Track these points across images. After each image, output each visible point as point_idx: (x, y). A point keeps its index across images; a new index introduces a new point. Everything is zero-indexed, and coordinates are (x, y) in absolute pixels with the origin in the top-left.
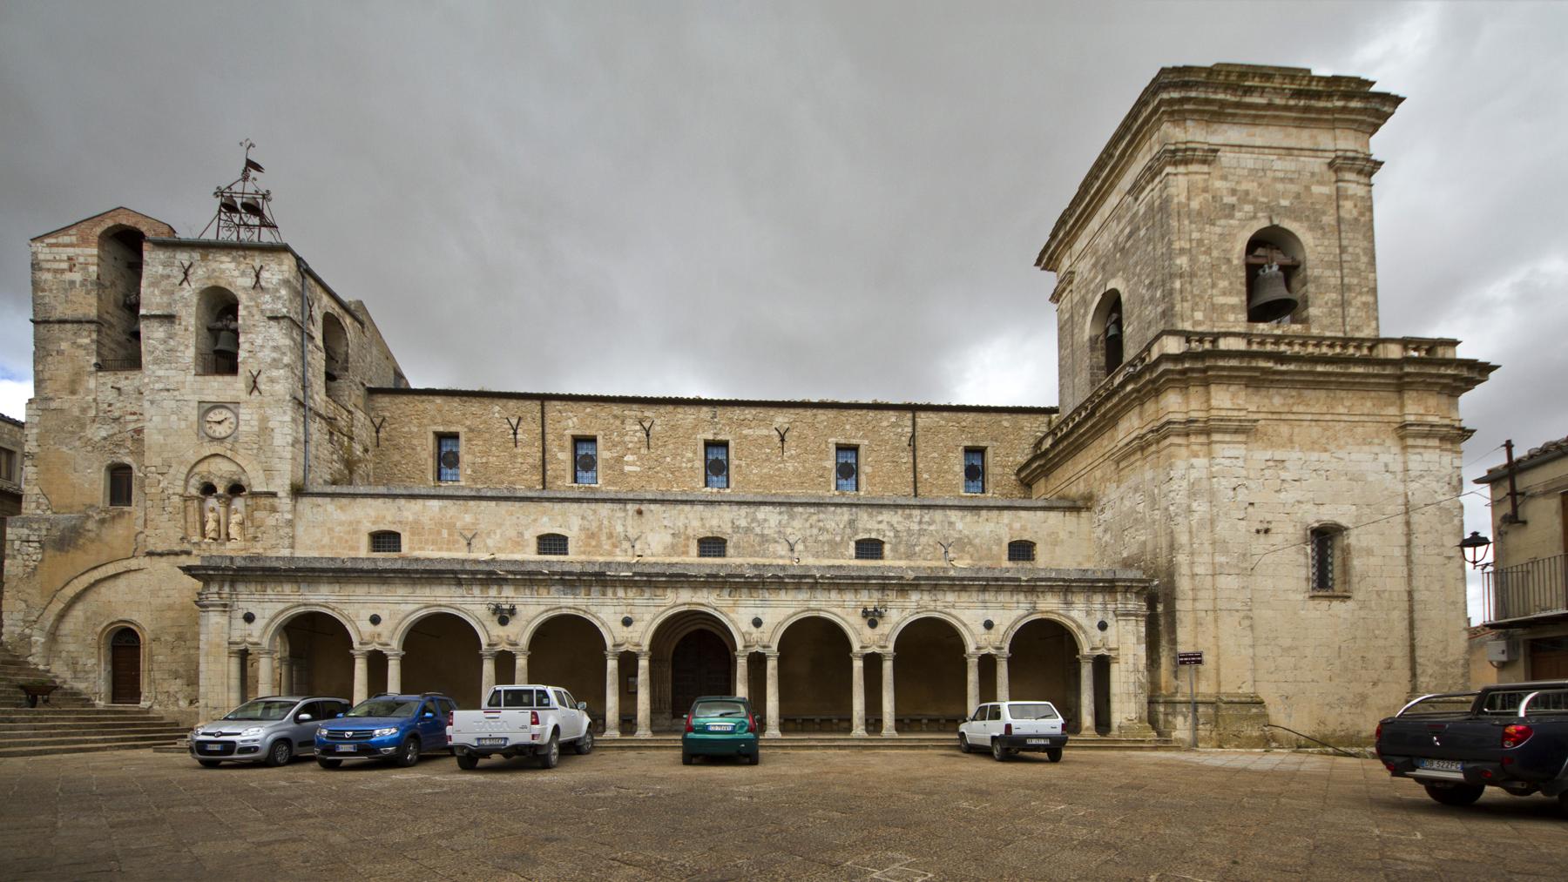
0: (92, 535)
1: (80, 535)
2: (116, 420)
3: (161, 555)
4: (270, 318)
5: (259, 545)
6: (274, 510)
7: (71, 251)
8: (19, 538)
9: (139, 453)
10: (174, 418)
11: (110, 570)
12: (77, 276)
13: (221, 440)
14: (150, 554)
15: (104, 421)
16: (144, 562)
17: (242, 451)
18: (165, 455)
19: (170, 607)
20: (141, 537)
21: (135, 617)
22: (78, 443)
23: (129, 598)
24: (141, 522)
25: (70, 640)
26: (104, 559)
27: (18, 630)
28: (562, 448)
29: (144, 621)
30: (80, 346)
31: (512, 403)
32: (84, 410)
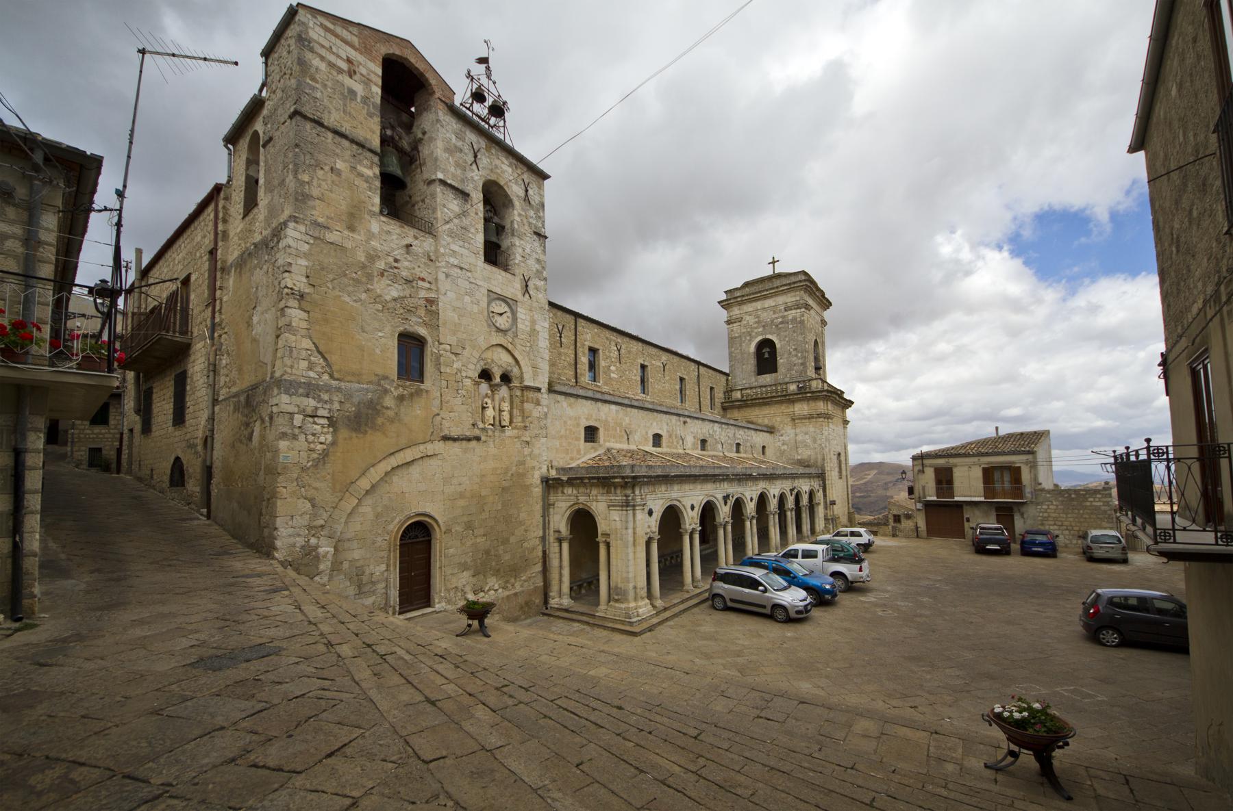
0: (390, 413)
1: (378, 412)
2: (408, 281)
3: (455, 440)
4: (535, 233)
5: (527, 433)
6: (538, 403)
7: (353, 54)
8: (302, 411)
9: (435, 327)
10: (467, 299)
11: (408, 455)
12: (359, 89)
13: (504, 332)
14: (446, 438)
15: (395, 279)
16: (439, 446)
17: (519, 347)
19: (462, 495)
20: (438, 418)
21: (429, 509)
22: (364, 296)
24: (437, 402)
25: (355, 544)
26: (403, 441)
27: (300, 541)
29: (435, 509)
30: (360, 175)
31: (559, 313)
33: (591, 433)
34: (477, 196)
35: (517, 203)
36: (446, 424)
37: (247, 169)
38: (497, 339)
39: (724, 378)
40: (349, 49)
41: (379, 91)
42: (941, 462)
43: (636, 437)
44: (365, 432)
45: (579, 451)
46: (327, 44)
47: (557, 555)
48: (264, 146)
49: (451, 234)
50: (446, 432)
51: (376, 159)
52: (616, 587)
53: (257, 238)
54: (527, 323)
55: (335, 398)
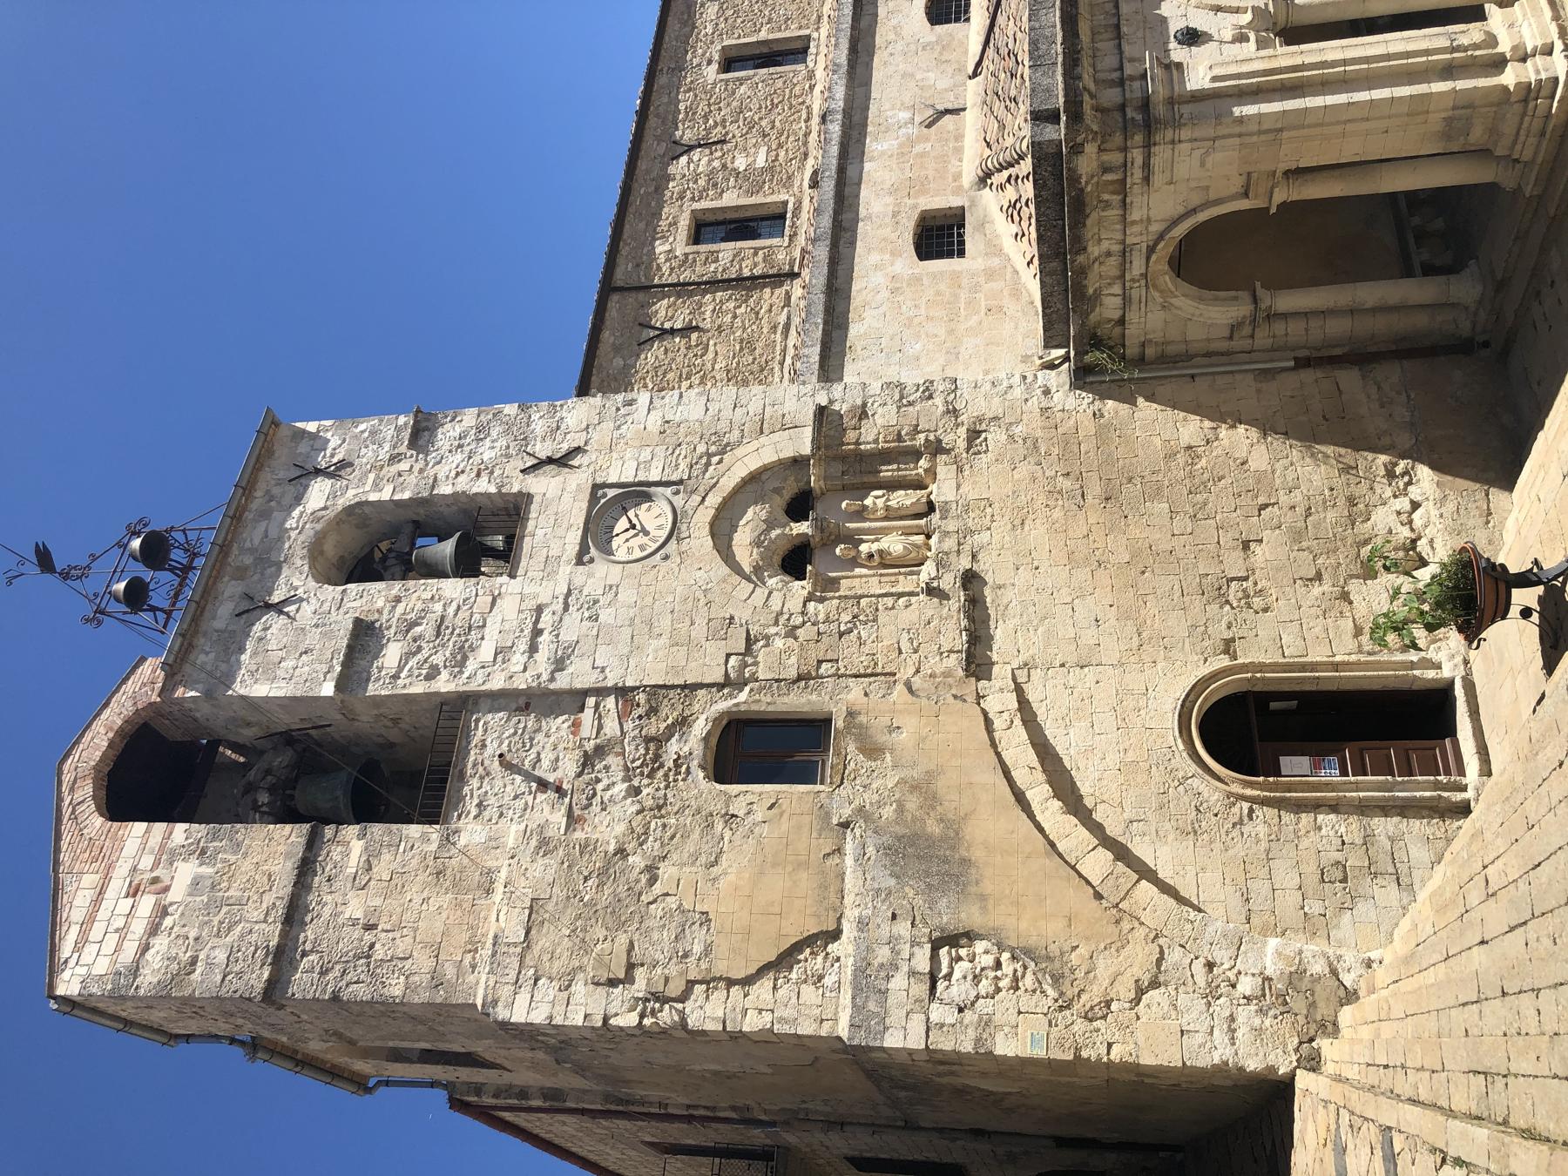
7: (117, 885)
12: (186, 872)
18: (699, 631)
20: (917, 682)
23: (1107, 721)
28: (713, 257)
32: (545, 846)
35: (350, 496)
36: (934, 664)
38: (699, 538)
40: (110, 894)
41: (180, 828)
43: (941, 85)
44: (965, 862)
45: (990, 274)
46: (112, 940)
47: (1314, 323)
49: (459, 660)
50: (954, 662)
51: (329, 831)
52: (1447, 136)
54: (646, 454)
55: (885, 930)
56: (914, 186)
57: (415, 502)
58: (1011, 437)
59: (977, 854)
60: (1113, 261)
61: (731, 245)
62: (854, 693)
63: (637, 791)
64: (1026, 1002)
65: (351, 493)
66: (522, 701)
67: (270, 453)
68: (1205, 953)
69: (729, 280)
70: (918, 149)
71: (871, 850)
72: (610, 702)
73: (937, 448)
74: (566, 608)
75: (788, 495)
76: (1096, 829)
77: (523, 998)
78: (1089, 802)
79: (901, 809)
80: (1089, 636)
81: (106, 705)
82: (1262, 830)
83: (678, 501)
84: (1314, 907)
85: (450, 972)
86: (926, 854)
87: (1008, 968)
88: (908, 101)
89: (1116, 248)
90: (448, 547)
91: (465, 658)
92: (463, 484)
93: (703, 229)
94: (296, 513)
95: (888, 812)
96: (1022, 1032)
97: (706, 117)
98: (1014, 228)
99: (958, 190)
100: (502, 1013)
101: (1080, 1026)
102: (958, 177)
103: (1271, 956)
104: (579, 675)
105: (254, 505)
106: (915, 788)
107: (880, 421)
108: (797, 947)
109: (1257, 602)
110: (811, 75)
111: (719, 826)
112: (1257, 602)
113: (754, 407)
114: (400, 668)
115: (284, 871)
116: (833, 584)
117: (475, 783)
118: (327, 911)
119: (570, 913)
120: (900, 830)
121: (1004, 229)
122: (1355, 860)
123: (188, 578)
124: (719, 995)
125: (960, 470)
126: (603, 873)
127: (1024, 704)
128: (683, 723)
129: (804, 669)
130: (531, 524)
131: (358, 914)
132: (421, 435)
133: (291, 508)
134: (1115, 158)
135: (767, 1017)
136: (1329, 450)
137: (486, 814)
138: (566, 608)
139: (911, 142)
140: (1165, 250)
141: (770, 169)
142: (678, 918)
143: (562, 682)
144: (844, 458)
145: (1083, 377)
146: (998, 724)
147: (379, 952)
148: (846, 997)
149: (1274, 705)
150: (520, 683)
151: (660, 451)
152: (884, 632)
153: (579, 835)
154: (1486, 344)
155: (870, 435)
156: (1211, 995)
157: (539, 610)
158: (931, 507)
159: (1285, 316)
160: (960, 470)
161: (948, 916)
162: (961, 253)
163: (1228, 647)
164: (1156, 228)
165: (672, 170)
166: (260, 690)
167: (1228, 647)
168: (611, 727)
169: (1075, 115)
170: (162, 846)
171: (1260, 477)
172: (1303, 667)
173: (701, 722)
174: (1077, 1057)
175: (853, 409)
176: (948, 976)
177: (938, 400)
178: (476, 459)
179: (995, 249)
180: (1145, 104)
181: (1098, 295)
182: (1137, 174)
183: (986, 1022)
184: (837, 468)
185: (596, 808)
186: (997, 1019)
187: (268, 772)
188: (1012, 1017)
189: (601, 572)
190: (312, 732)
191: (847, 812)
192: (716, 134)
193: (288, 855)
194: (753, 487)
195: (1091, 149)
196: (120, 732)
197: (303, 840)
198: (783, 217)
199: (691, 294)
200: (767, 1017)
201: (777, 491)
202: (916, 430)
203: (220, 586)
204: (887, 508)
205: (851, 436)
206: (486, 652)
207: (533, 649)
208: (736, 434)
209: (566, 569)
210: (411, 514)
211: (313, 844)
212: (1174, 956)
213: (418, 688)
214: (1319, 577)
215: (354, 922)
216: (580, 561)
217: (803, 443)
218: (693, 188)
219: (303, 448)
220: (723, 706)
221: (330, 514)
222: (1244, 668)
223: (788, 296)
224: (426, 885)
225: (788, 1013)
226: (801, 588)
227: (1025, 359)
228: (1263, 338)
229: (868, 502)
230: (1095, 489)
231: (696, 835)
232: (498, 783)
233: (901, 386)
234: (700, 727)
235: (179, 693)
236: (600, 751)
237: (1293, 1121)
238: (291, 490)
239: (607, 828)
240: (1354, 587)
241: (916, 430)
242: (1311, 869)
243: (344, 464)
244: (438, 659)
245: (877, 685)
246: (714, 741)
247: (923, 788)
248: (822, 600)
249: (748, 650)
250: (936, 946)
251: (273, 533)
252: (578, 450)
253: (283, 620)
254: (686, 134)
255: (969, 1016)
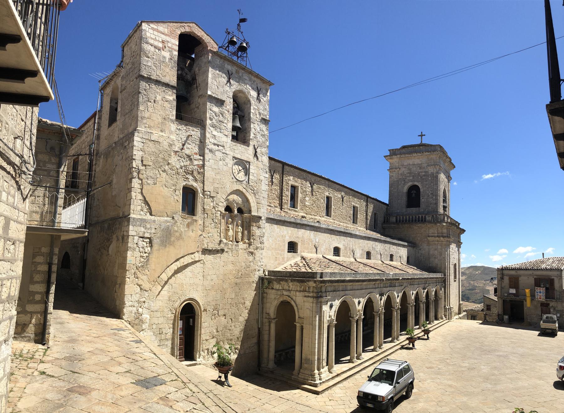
12: (167, 55)
20: (202, 237)
28: (287, 190)
32: (170, 145)
33: (292, 247)
34: (229, 106)
35: (252, 102)
36: (206, 241)
37: (111, 103)
39: (386, 207)
42: (513, 273)
43: (322, 249)
45: (283, 258)
47: (267, 332)
48: (121, 92)
49: (214, 126)
51: (175, 91)
53: (116, 139)
54: (255, 175)
55: (153, 227)
56: (303, 241)
57: (249, 119)
58: (250, 262)
59: (167, 249)
60: (287, 288)
61: (290, 195)
62: (200, 222)
63: (181, 168)
64: (138, 259)
65: (253, 102)
66: (203, 141)
67: (264, 83)
68: (147, 301)
69: (282, 193)
70: (310, 243)
71: (168, 224)
72: (201, 163)
73: (250, 244)
74: (223, 153)
75: (243, 208)
76: (171, 278)
77: (139, 139)
78: (176, 276)
79: (176, 231)
80: (209, 278)
81: (208, 35)
82: (169, 316)
83: (244, 182)
84: (154, 326)
85: (145, 121)
86: (168, 237)
87: (145, 255)
88: (321, 241)
89: (290, 289)
90: (238, 125)
91: (214, 127)
92: (253, 130)
93: (294, 188)
94: (250, 88)
95: (176, 228)
96: (133, 258)
97: (318, 191)
98: (293, 265)
99: (301, 252)
100: (136, 134)
101: (133, 271)
102: (304, 252)
103: (146, 316)
104: (208, 155)
105: (252, 77)
106: (180, 235)
107: (257, 231)
108: (149, 205)
109: (213, 317)
110: (323, 217)
111: (174, 188)
112: (213, 317)
113: (263, 202)
114: (212, 111)
115: (166, 80)
116: (224, 218)
117: (185, 128)
118: (158, 90)
119: (157, 151)
120: (172, 231)
121: (292, 262)
122: (163, 336)
123: (235, 57)
124: (139, 186)
125: (245, 250)
126: (164, 159)
127: (196, 262)
128: (196, 180)
129: (206, 210)
130: (243, 146)
131: (157, 99)
132: (264, 121)
133: (251, 87)
134: (311, 290)
135: (134, 198)
136: (242, 335)
137: (177, 131)
138: (223, 153)
139: (312, 242)
140: (289, 299)
141: (305, 205)
142: (155, 177)
143: (207, 151)
144: (250, 222)
145: (261, 279)
146: (192, 256)
147: (149, 104)
148: (139, 217)
149: (191, 320)
150: (207, 141)
151: (256, 179)
152: (213, 230)
153: (173, 154)
154: (259, 370)
155: (254, 229)
156: (139, 302)
157: (223, 146)
158: (237, 242)
159: (270, 326)
160: (245, 250)
161: (156, 241)
162: (288, 252)
163: (205, 310)
164: (294, 298)
165: (308, 182)
166: (210, 75)
167: (205, 310)
168: (196, 163)
169: (322, 282)
170: (173, 49)
171: (238, 319)
172: (200, 327)
173: (196, 185)
174: (127, 270)
175: (260, 225)
176: (143, 241)
177: (260, 245)
178: (258, 134)
179: (288, 260)
180: (321, 297)
181: (280, 284)
182: (307, 294)
183: (134, 249)
184: (248, 220)
185: (179, 158)
186: (135, 252)
187: (186, 74)
188: (135, 256)
189: (231, 162)
190: (195, 86)
191: (176, 218)
192: (314, 193)
193: (170, 81)
194: (246, 200)
195: (314, 285)
196: (201, 38)
197: (173, 85)
198: (294, 207)
199: (280, 184)
200: (134, 198)
201: (244, 206)
202: (254, 240)
203: (235, 67)
204: (238, 232)
205: (254, 224)
206: (215, 133)
207: (215, 144)
208: (257, 197)
209: (232, 154)
210: (246, 115)
211: (172, 87)
212: (146, 294)
213: (208, 115)
214: (218, 332)
215: (156, 98)
216: (233, 157)
217: (254, 213)
218: (304, 186)
219: (264, 91)
220: (199, 190)
221: (249, 96)
222: (201, 314)
223: (277, 207)
224: (162, 115)
225: (135, 203)
226: (223, 210)
227: (266, 266)
228: (265, 320)
229: (240, 227)
230: (238, 281)
231: (172, 182)
232: (184, 134)
233: (263, 237)
234: (195, 184)
235: (210, 55)
236: (191, 160)
237: (108, 317)
238: (255, 87)
239: (174, 160)
240: (215, 340)
241: (254, 240)
242: (161, 326)
243: (260, 101)
244: (214, 121)
245: (201, 227)
246: (191, 187)
247: (180, 238)
248: (220, 215)
249: (211, 197)
250: (149, 238)
251: (246, 81)
252: (258, 159)
253: (226, 82)
254: (315, 187)
255: (135, 245)
